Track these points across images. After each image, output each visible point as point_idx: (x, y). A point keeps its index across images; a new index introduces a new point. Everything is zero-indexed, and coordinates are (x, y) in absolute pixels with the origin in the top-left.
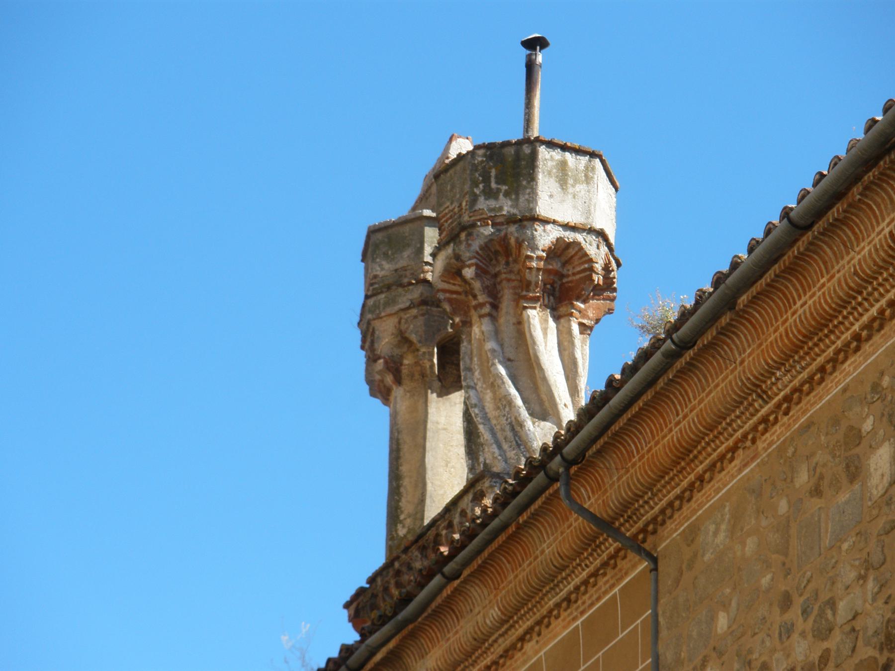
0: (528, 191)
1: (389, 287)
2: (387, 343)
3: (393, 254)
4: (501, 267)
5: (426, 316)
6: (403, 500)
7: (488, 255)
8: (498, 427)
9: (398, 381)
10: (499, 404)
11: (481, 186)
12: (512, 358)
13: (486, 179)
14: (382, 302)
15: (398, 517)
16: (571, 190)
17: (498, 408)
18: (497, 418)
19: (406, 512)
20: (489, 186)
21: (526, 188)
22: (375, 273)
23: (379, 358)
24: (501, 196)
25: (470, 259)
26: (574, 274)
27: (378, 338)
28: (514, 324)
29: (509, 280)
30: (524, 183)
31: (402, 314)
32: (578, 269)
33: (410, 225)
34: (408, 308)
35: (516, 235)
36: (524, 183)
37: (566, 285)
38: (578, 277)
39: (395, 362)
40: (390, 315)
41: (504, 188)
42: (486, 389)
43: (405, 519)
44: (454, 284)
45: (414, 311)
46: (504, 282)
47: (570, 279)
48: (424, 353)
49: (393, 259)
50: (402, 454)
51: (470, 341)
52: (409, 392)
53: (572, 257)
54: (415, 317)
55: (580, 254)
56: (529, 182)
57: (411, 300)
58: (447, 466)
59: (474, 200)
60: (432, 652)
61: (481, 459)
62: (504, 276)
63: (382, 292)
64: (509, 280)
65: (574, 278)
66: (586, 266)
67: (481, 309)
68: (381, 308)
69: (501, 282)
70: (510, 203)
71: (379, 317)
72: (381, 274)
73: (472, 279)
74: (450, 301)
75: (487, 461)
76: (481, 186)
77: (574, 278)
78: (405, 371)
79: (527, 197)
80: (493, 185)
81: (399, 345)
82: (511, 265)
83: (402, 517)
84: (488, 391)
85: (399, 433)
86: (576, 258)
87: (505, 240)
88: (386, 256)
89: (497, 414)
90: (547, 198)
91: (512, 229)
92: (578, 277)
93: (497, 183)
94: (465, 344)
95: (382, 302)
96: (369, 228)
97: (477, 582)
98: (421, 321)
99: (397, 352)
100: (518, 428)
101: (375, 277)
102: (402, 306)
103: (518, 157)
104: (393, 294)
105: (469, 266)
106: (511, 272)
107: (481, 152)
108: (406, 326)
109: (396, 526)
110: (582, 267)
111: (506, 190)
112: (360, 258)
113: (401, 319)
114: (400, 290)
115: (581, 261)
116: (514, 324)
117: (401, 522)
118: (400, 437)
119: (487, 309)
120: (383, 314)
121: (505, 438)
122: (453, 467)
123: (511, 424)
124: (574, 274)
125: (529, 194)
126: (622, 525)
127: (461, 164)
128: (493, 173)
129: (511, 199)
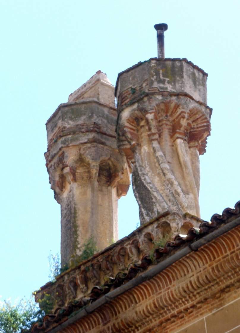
0: (180, 82)
1: (74, 133)
2: (72, 159)
3: (75, 117)
4: (163, 117)
5: (96, 148)
6: (79, 237)
7: (159, 110)
8: (164, 194)
9: (75, 180)
10: (164, 184)
11: (155, 77)
12: (170, 161)
13: (158, 74)
14: (69, 139)
15: (76, 246)
16: (198, 87)
17: (164, 185)
18: (163, 190)
19: (81, 244)
20: (159, 77)
21: (179, 81)
22: (64, 126)
23: (67, 166)
24: (166, 83)
25: (151, 109)
26: (198, 128)
27: (67, 156)
28: (170, 146)
29: (167, 125)
30: (178, 78)
31: (81, 146)
32: (200, 125)
33: (85, 105)
34: (85, 143)
35: (176, 101)
36: (178, 78)
37: (193, 133)
38: (200, 129)
39: (73, 170)
40: (75, 146)
41: (167, 79)
42: (155, 176)
43: (81, 247)
44: (132, 125)
45: (89, 145)
46: (164, 125)
47: (195, 130)
48: (94, 166)
49: (76, 120)
50: (77, 215)
51: (140, 154)
52: (80, 185)
53: (198, 119)
54: (90, 148)
55: (203, 117)
56: (181, 78)
57: (88, 139)
58: (103, 223)
59: (152, 83)
60: (142, 302)
61: (155, 209)
62: (164, 122)
63: (70, 134)
64: (167, 125)
65: (198, 129)
66: (205, 124)
67: (153, 136)
68: (69, 142)
69: (162, 125)
70: (171, 86)
71: (68, 146)
72: (68, 126)
73: (152, 120)
74: (131, 133)
75: (159, 211)
76: (155, 77)
77: (198, 129)
78: (78, 175)
79: (180, 85)
80: (161, 77)
81: (76, 162)
82: (169, 117)
83: (79, 246)
84: (156, 177)
85: (75, 205)
86: (200, 120)
87: (167, 105)
88: (71, 119)
89: (163, 188)
90: (189, 87)
91: (174, 98)
92: (200, 129)
93: (163, 76)
94: (138, 155)
95: (69, 139)
96: (61, 104)
97: (197, 257)
98: (93, 149)
99: (74, 165)
100: (176, 196)
101: (65, 127)
102: (82, 142)
103: (173, 66)
104: (77, 136)
105: (151, 113)
106: (168, 120)
107: (154, 62)
108: (84, 152)
109: (75, 250)
110: (203, 125)
111: (168, 81)
112: (46, 122)
113: (80, 148)
114: (81, 134)
115: (202, 122)
116: (170, 146)
117: (78, 248)
118: (76, 207)
119: (157, 136)
120: (70, 145)
121: (169, 200)
122: (106, 225)
123: (172, 193)
124: (198, 128)
125: (181, 83)
126: (27, 326)
127: (141, 67)
128: (161, 72)
129: (172, 85)
